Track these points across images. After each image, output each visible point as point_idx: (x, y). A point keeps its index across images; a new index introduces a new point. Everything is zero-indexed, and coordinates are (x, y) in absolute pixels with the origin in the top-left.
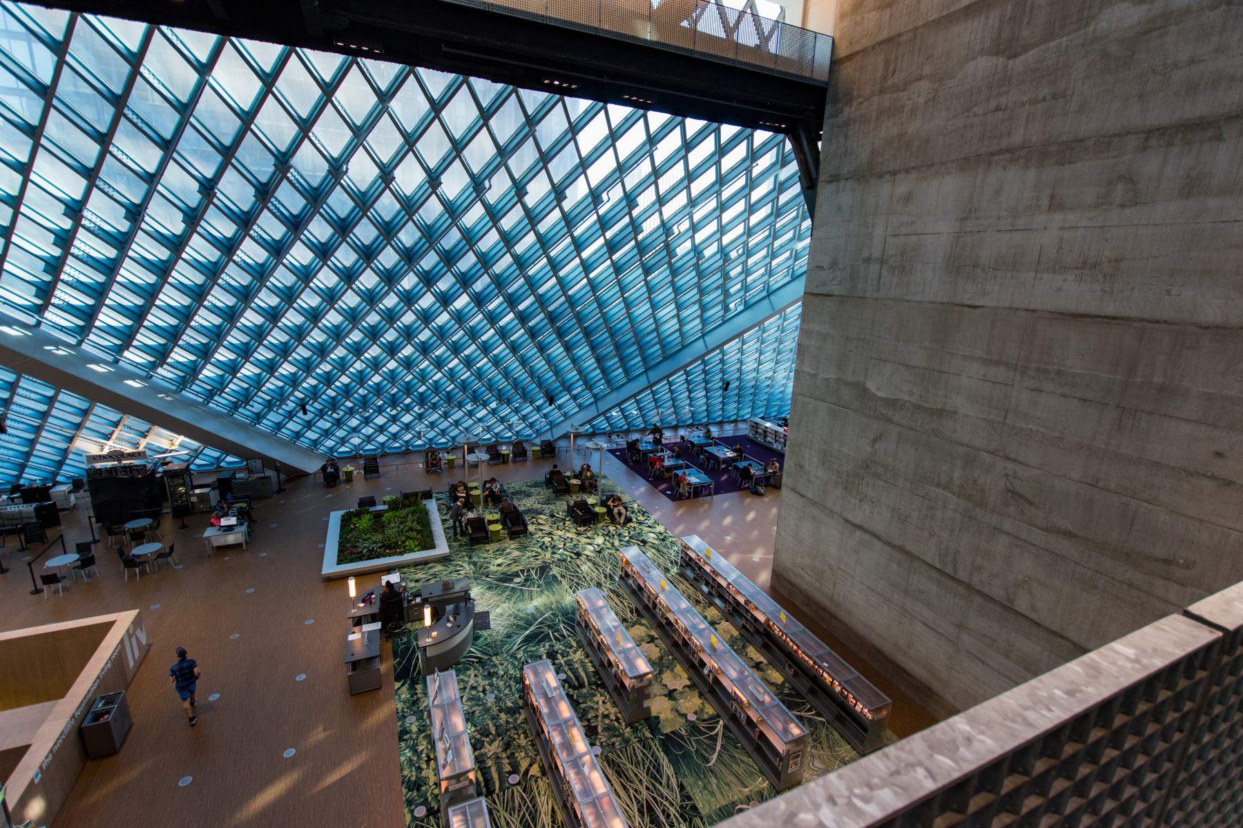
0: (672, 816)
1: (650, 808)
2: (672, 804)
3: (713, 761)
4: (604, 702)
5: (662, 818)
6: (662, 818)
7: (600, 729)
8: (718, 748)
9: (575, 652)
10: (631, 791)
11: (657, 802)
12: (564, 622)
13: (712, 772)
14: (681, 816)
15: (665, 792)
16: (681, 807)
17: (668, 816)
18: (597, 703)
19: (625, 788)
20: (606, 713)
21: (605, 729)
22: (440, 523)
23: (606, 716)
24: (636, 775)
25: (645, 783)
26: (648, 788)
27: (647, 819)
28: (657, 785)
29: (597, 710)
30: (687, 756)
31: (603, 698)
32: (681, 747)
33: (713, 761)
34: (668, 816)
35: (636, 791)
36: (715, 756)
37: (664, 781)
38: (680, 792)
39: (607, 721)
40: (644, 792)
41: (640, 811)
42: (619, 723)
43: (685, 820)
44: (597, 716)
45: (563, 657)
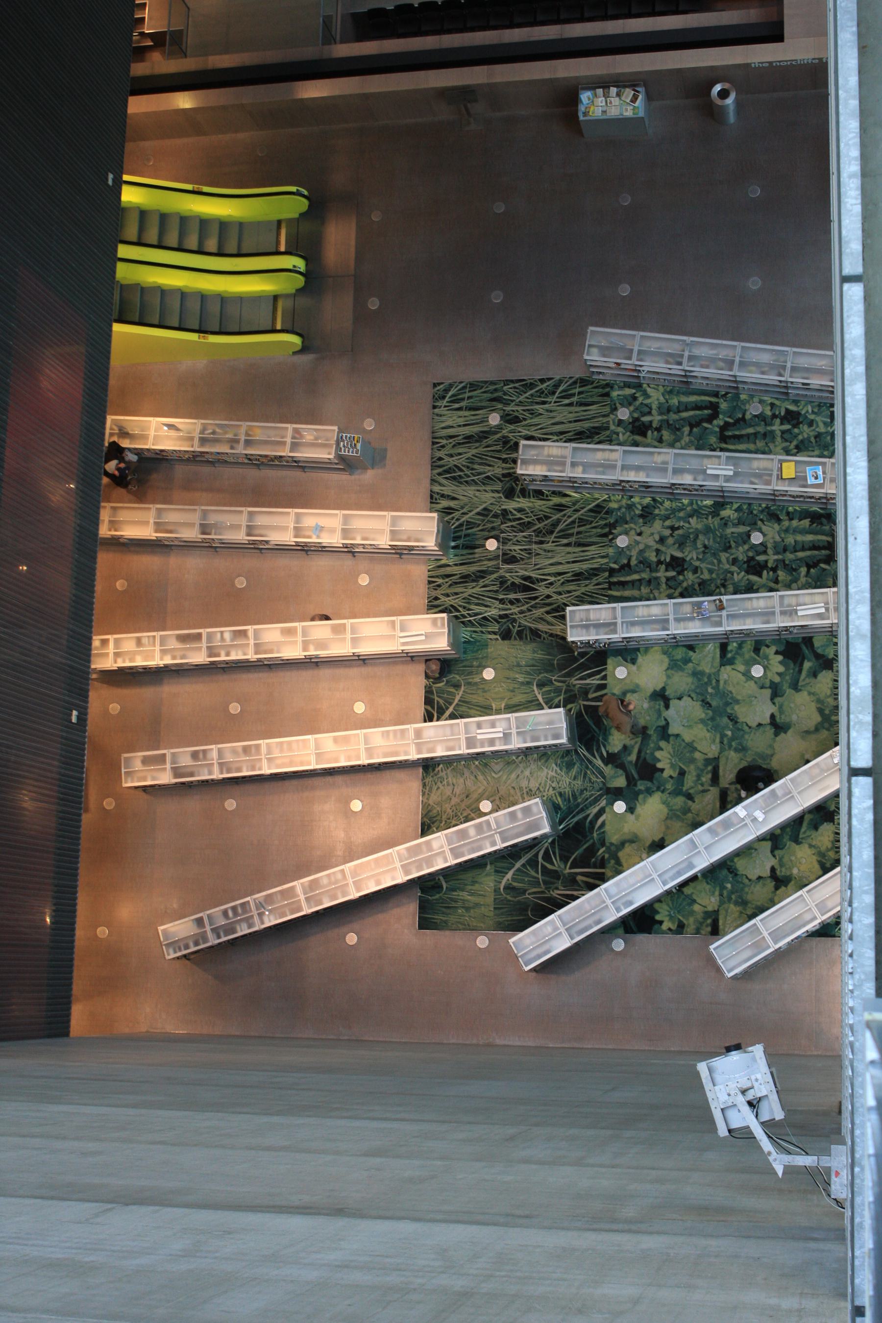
0: (509, 606)
1: (527, 589)
2: (521, 612)
3: (536, 692)
4: (640, 534)
5: (512, 596)
6: (512, 596)
7: (678, 554)
10: (552, 579)
11: (530, 598)
13: (528, 683)
14: (506, 616)
15: (539, 612)
16: (514, 620)
17: (511, 602)
20: (657, 538)
23: (662, 540)
24: (569, 592)
25: (555, 597)
26: (548, 597)
27: (518, 581)
28: (548, 608)
29: (647, 547)
31: (632, 532)
32: (561, 667)
33: (536, 692)
34: (511, 602)
35: (551, 584)
37: (549, 618)
38: (530, 629)
39: (670, 541)
40: (547, 592)
42: (678, 528)
43: (501, 617)
44: (658, 551)
45: (668, 579)
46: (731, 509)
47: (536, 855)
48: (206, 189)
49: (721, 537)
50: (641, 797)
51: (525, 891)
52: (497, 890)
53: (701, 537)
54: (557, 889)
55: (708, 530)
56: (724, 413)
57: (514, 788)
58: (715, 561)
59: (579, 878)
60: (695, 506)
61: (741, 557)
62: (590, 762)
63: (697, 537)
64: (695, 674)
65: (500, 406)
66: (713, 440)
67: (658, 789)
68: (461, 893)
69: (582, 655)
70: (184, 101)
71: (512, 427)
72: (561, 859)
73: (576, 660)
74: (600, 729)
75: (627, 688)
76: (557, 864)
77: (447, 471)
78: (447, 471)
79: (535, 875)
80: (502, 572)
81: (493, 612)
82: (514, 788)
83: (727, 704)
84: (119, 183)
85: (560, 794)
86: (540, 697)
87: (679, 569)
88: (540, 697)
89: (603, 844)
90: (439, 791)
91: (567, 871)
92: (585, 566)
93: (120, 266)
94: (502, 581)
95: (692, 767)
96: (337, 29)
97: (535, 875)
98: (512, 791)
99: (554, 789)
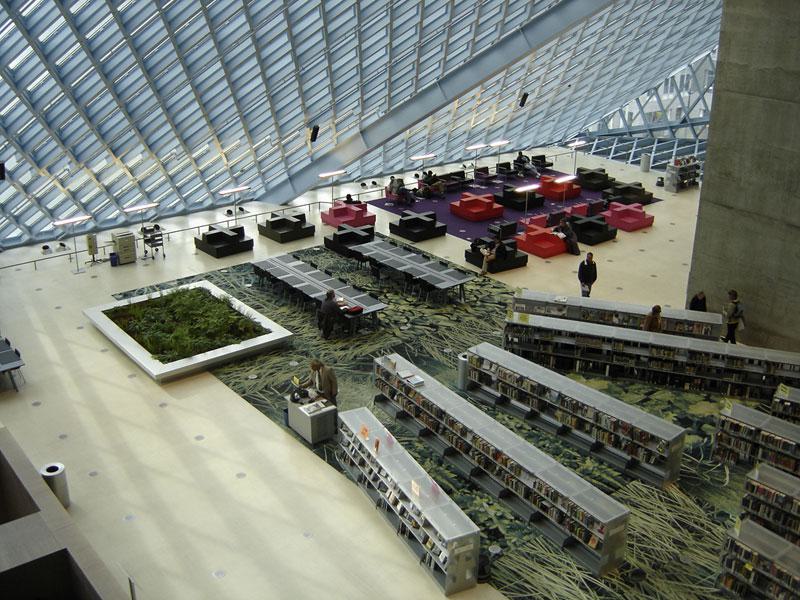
8: (728, 472)
9: (584, 462)
10: (564, 575)
12: (267, 405)
18: (482, 506)
19: (556, 574)
20: (499, 514)
21: (508, 530)
22: (372, 350)
23: (502, 517)
27: (593, 593)
28: (676, 506)
30: (705, 486)
35: (568, 573)
36: (727, 478)
37: (681, 503)
41: (582, 587)
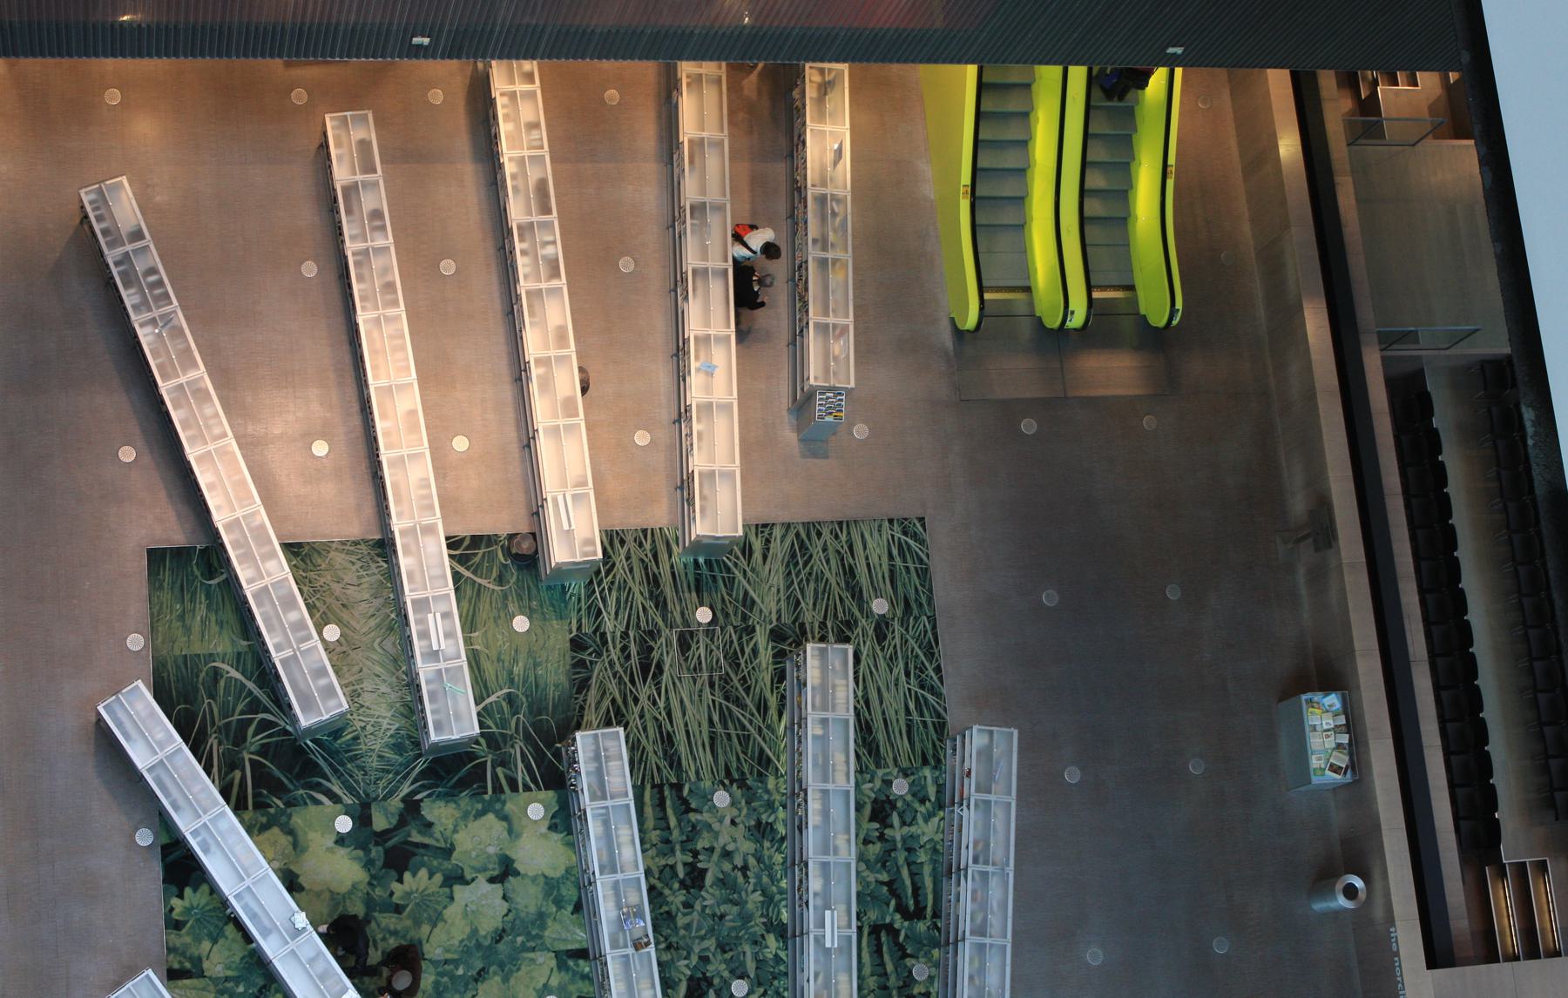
2: (611, 664)
10: (661, 704)
16: (599, 655)
26: (636, 700)
33: (500, 693)
34: (624, 649)
43: (603, 635)
44: (711, 850)
46: (778, 948)
47: (266, 710)
48: (1170, 183)
49: (737, 937)
50: (360, 853)
51: (212, 696)
52: (211, 657)
53: (736, 909)
54: (220, 743)
55: (746, 918)
56: (910, 928)
57: (361, 671)
58: (703, 932)
59: (237, 774)
60: (778, 897)
61: (711, 968)
62: (405, 778)
63: (736, 903)
64: (541, 917)
65: (899, 613)
66: (873, 915)
67: (373, 877)
68: (203, 607)
69: (557, 754)
70: (1289, 146)
71: (871, 632)
72: (263, 746)
73: (549, 745)
74: (453, 787)
75: (515, 821)
76: (254, 741)
77: (802, 546)
78: (802, 546)
79: (238, 711)
80: (665, 632)
81: (609, 625)
82: (361, 671)
83: (502, 966)
84: (1171, 63)
85: (356, 738)
86: (492, 699)
87: (688, 882)
88: (492, 699)
89: (289, 804)
90: (350, 565)
91: (247, 756)
92: (683, 749)
93: (1057, 70)
94: (653, 634)
95: (408, 923)
96: (1401, 351)
97: (238, 711)
98: (356, 669)
99: (364, 728)
